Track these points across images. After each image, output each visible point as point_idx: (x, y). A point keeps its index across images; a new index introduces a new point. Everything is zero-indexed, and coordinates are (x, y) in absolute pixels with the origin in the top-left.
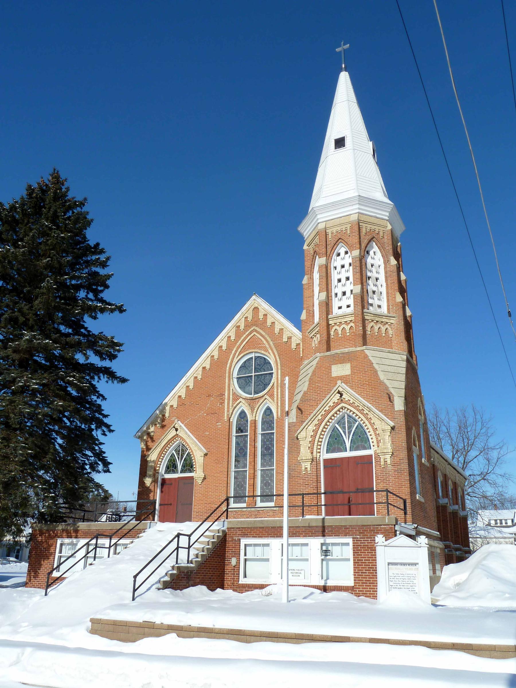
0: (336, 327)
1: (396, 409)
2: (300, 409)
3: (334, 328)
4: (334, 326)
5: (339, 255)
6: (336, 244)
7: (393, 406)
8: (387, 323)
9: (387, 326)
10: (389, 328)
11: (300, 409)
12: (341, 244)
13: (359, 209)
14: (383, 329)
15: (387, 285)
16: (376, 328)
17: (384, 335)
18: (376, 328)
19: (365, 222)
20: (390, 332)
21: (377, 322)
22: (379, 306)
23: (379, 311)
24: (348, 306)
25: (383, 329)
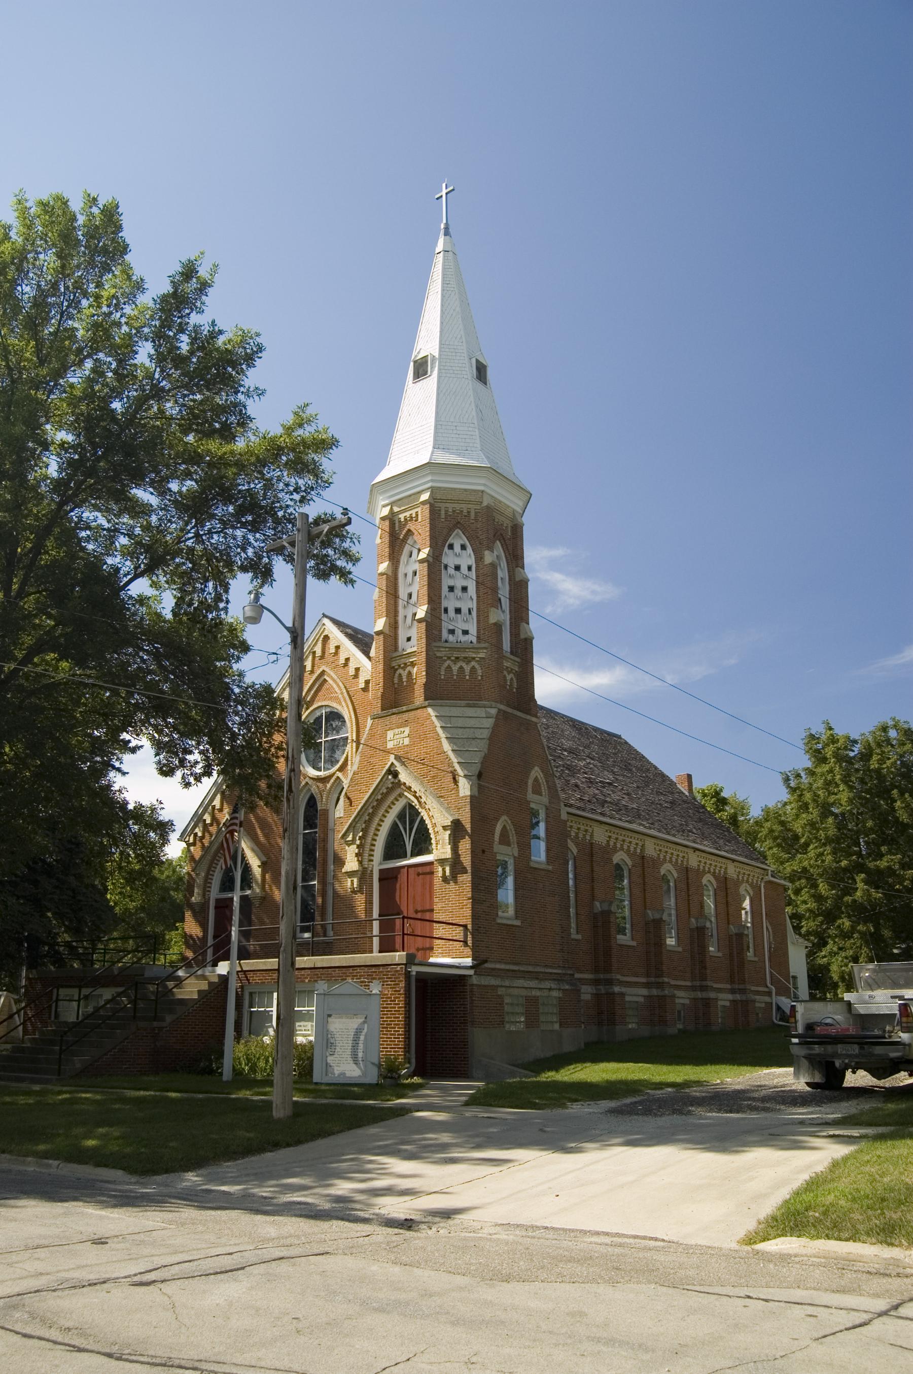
0: (400, 671)
1: (461, 795)
2: (349, 798)
3: (446, 664)
4: (445, 661)
5: (451, 547)
6: (450, 531)
7: (458, 791)
8: (474, 658)
9: (473, 663)
10: (477, 666)
11: (349, 798)
12: (457, 531)
13: (432, 481)
14: (467, 669)
15: (478, 597)
16: (455, 668)
17: (467, 677)
18: (455, 668)
19: (442, 501)
20: (480, 672)
21: (457, 658)
22: (465, 632)
23: (464, 638)
24: (465, 632)
25: (467, 669)
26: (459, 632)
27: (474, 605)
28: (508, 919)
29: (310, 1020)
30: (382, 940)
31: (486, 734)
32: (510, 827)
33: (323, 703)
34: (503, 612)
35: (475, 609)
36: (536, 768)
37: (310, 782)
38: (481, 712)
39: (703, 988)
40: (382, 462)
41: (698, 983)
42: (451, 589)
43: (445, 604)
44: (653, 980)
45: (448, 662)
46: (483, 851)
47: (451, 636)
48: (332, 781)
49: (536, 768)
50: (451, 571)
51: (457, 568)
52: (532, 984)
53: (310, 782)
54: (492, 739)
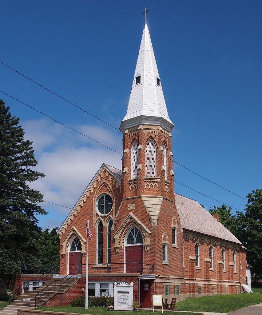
26: (151, 173)
27: (155, 164)
28: (165, 263)
29: (155, 306)
30: (78, 248)
31: (160, 206)
32: (167, 235)
33: (103, 193)
34: (165, 166)
35: (156, 165)
36: (174, 217)
37: (100, 218)
38: (158, 199)
39: (220, 282)
40: (124, 113)
41: (219, 280)
42: (148, 159)
43: (146, 164)
44: (206, 279)
45: (147, 183)
46: (159, 243)
47: (148, 174)
48: (108, 217)
49: (174, 217)
50: (148, 152)
51: (150, 151)
52: (177, 281)
53: (100, 218)
54: (161, 208)
